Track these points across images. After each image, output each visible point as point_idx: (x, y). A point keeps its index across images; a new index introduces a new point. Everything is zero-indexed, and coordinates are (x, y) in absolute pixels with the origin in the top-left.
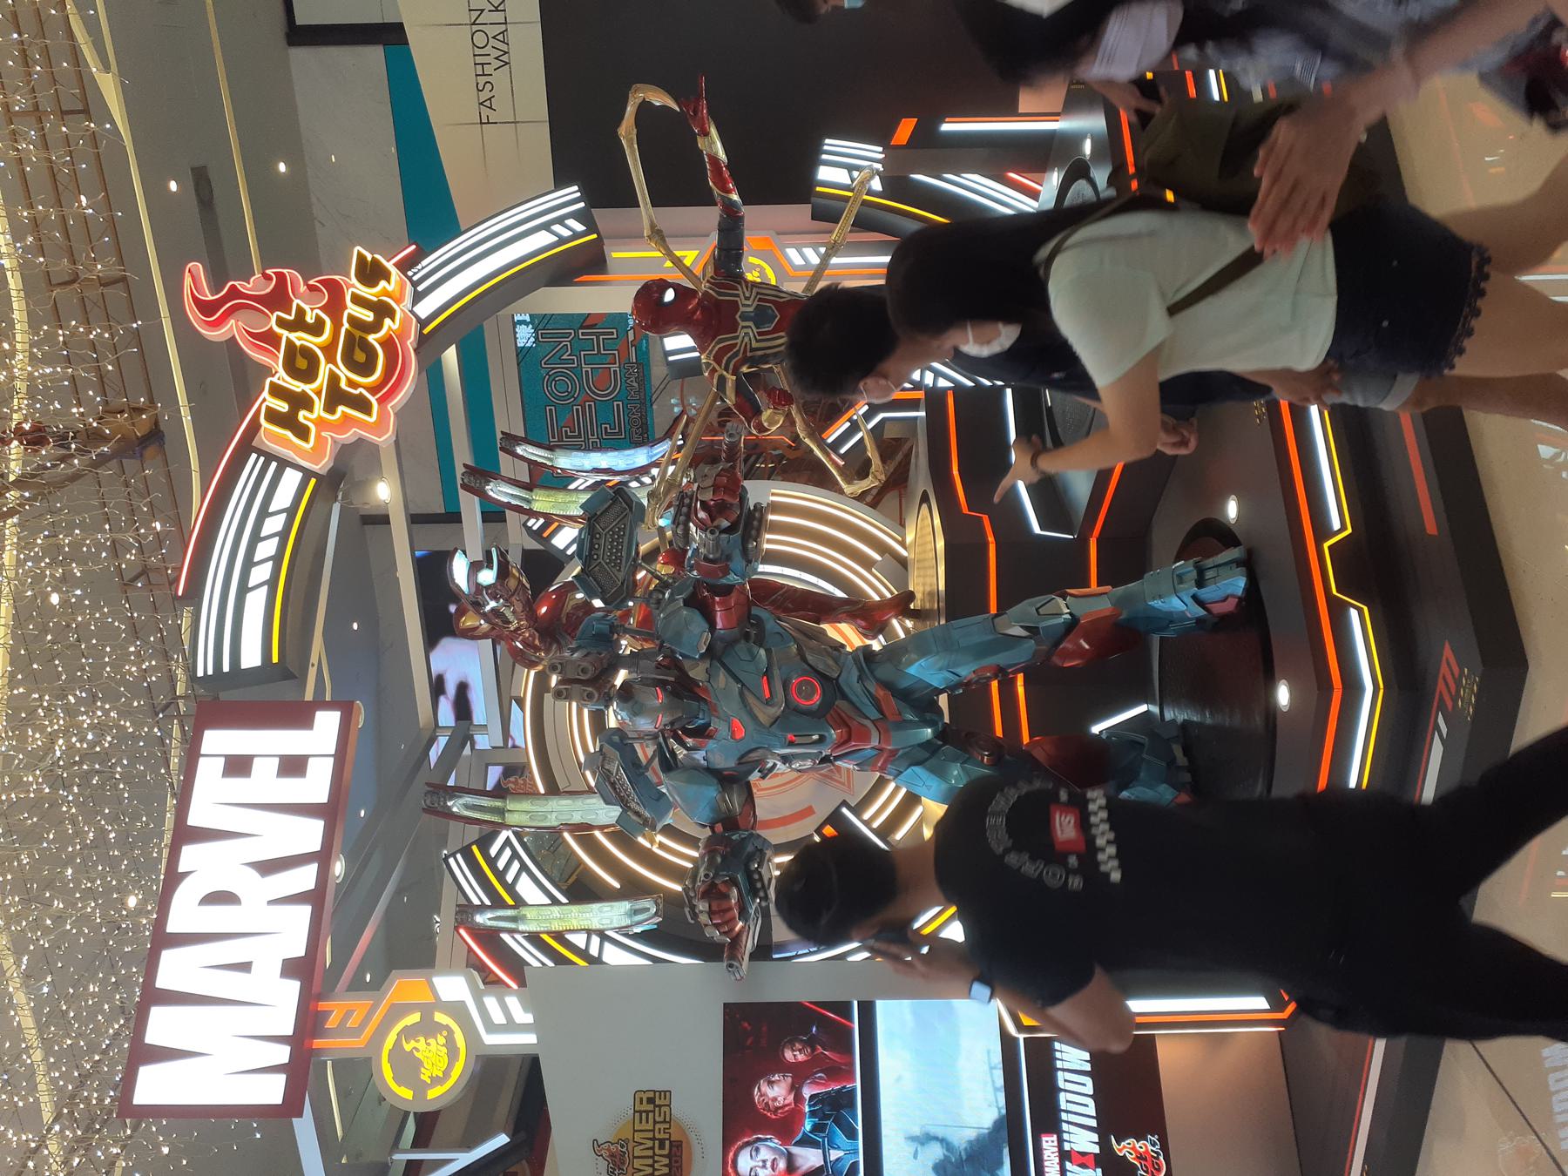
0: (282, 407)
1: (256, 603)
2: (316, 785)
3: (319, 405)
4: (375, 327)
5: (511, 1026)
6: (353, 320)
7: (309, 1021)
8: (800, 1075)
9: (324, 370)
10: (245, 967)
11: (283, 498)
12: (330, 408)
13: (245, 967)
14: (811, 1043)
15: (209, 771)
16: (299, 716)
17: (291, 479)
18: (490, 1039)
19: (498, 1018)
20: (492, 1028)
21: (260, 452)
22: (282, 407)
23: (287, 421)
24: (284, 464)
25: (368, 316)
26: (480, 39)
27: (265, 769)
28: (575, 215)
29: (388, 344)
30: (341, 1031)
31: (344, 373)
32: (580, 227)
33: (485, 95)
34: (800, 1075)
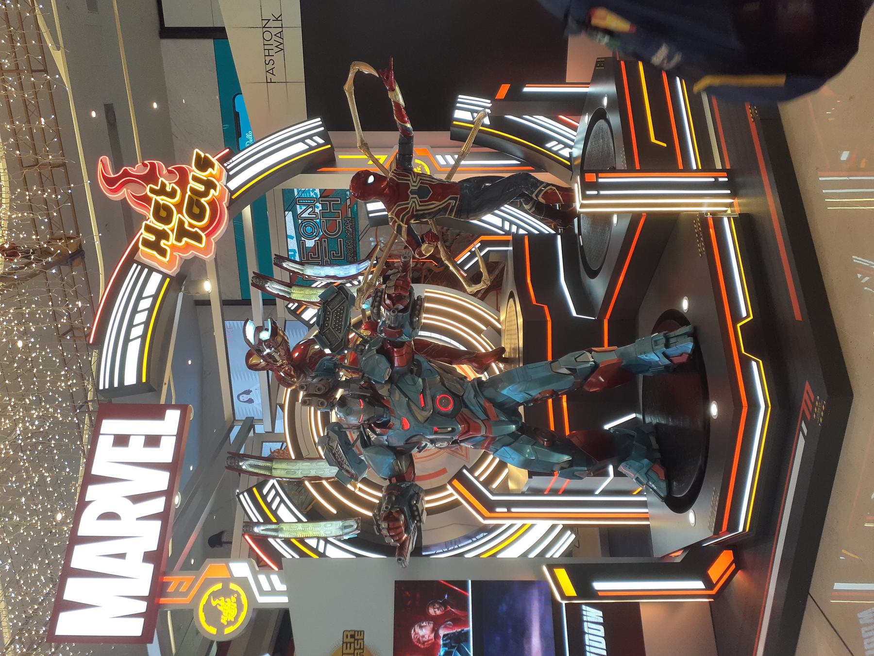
0: (152, 238)
1: (134, 348)
2: (165, 452)
3: (172, 237)
4: (205, 194)
5: (273, 592)
6: (193, 190)
7: (158, 587)
8: (437, 622)
9: (176, 217)
10: (122, 556)
11: (151, 288)
12: (179, 239)
13: (122, 556)
14: (444, 604)
15: (104, 443)
16: (156, 412)
17: (156, 278)
18: (262, 600)
19: (266, 587)
20: (262, 593)
21: (139, 263)
22: (152, 238)
23: (154, 246)
24: (152, 270)
25: (201, 188)
26: (267, 36)
27: (137, 442)
28: (319, 134)
29: (212, 204)
30: (177, 593)
31: (187, 219)
32: (321, 141)
33: (269, 67)
34: (437, 622)
